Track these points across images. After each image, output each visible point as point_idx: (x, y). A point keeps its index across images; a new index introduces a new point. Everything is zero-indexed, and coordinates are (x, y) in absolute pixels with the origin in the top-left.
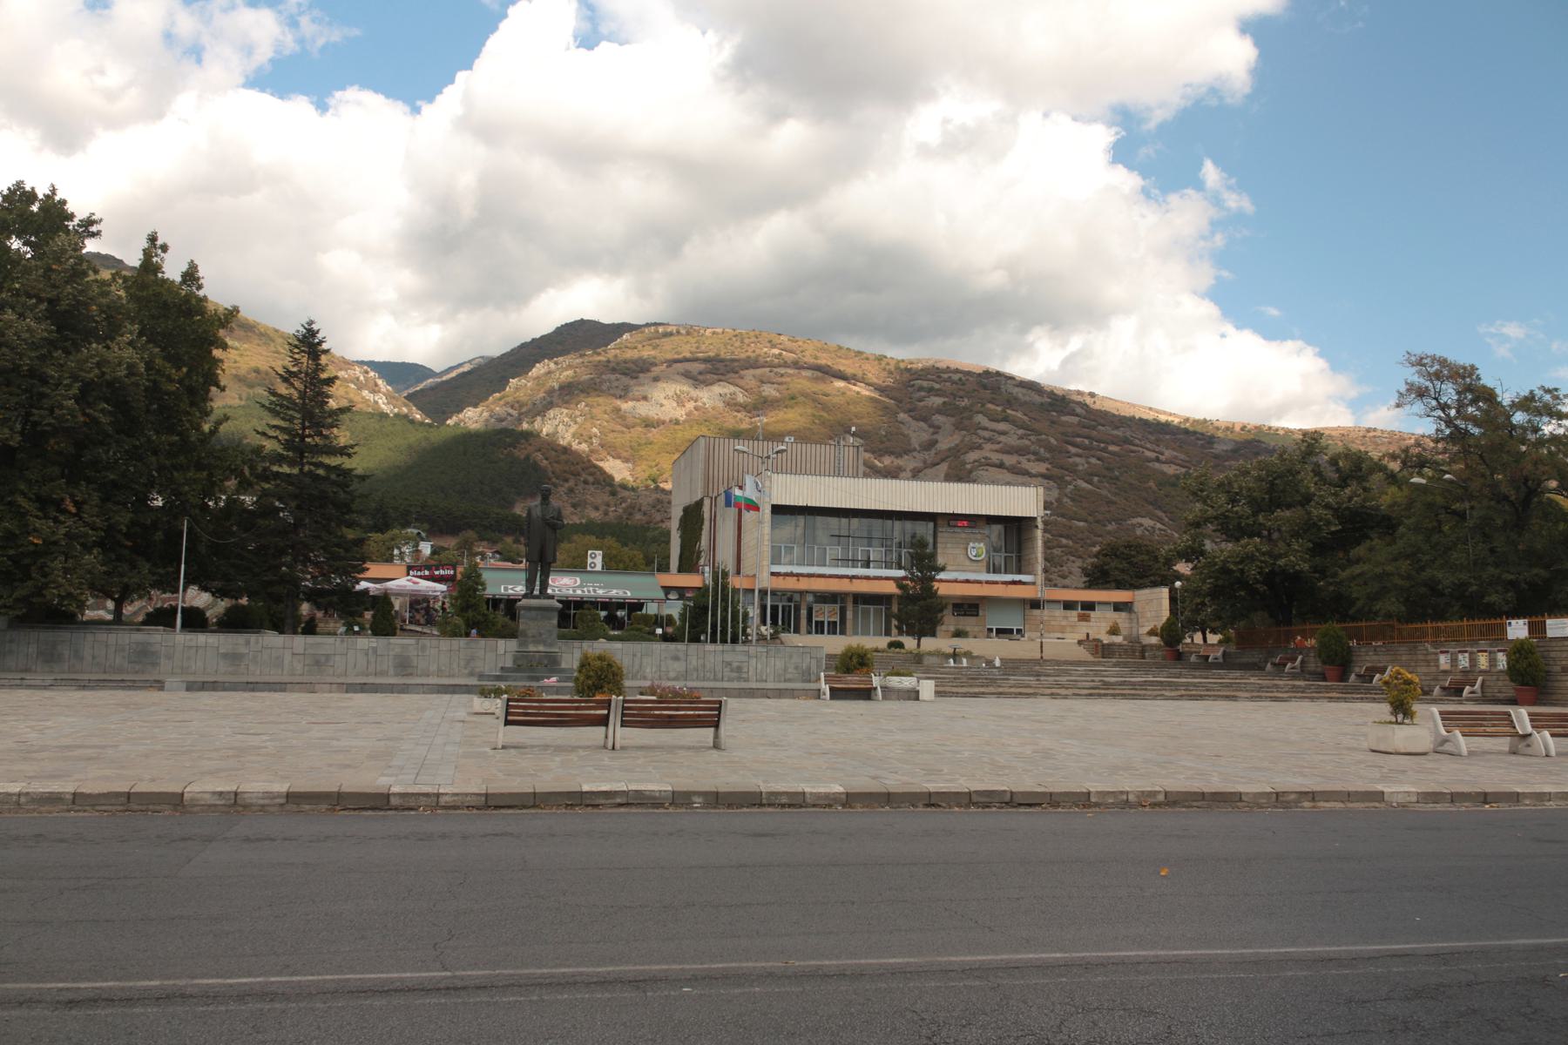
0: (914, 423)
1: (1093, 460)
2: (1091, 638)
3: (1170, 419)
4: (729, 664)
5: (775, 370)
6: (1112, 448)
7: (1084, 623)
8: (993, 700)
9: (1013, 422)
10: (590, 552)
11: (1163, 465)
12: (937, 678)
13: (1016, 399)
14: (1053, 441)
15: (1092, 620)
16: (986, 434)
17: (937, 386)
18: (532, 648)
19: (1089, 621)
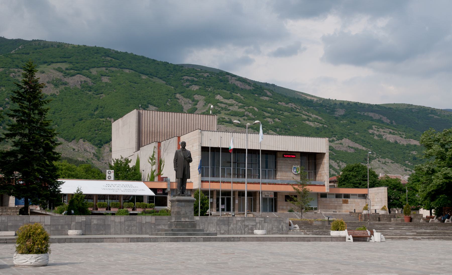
0: (185, 99)
1: (277, 120)
2: (356, 211)
3: (312, 98)
4: (247, 226)
5: (109, 68)
6: (286, 113)
7: (345, 204)
8: (412, 240)
9: (236, 99)
10: (107, 171)
11: (311, 123)
12: (382, 232)
13: (237, 87)
14: (256, 109)
15: (349, 203)
16: (223, 106)
17: (196, 79)
18: (183, 220)
19: (348, 203)
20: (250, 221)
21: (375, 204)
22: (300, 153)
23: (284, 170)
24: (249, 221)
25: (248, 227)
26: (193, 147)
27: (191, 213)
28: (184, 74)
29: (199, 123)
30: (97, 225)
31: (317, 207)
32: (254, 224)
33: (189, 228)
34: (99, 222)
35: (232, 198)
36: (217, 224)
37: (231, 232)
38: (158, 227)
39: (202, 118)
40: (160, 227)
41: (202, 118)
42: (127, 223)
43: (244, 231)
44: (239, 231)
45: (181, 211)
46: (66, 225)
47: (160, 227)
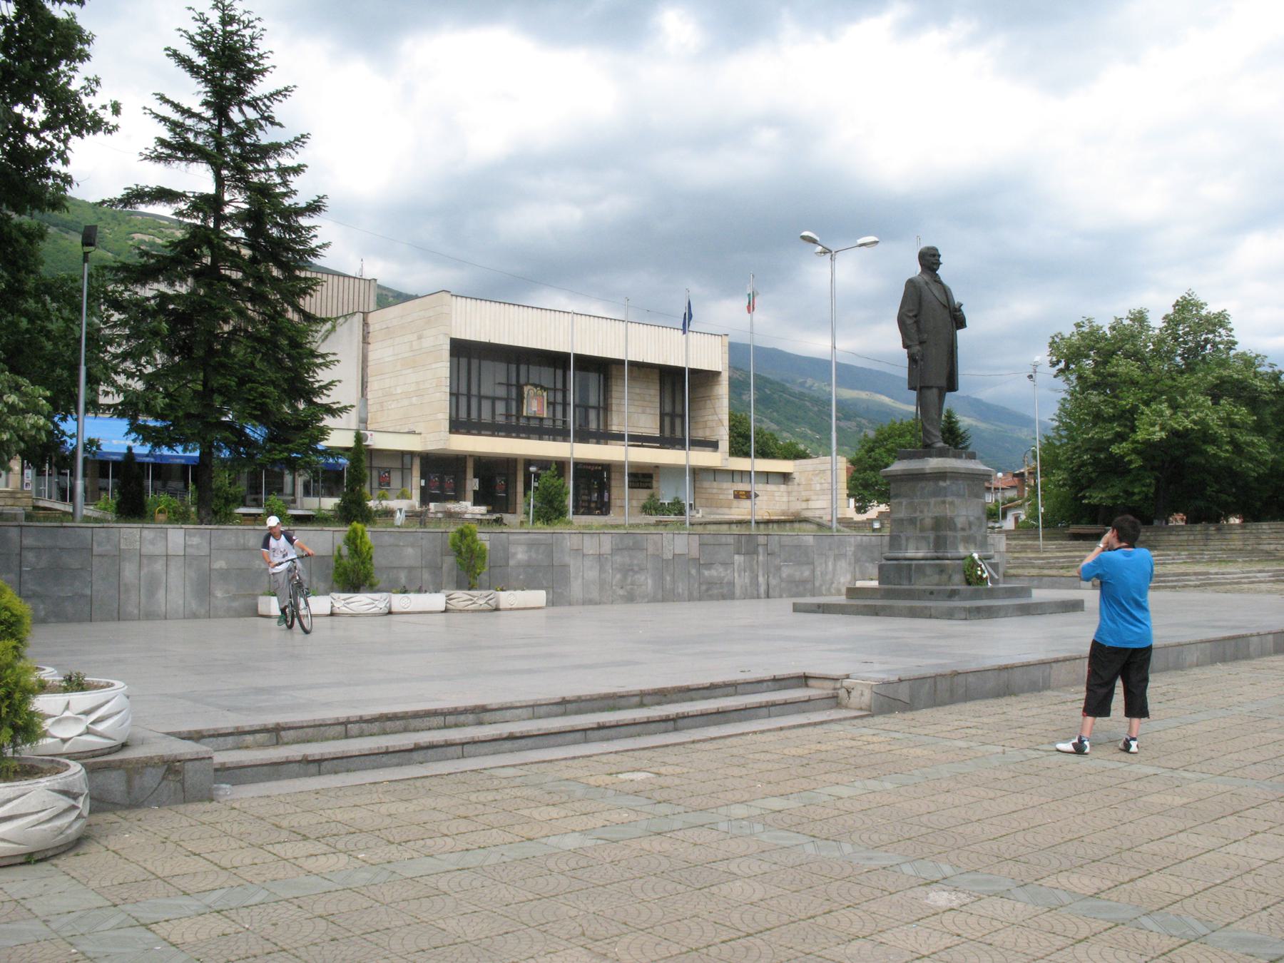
21: (813, 497)
22: (657, 371)
26: (420, 338)
28: (136, 229)
29: (335, 295)
30: (529, 566)
34: (534, 555)
36: (857, 560)
38: (706, 573)
39: (341, 284)
40: (714, 573)
41: (341, 284)
42: (618, 559)
45: (958, 516)
46: (424, 570)
47: (714, 573)
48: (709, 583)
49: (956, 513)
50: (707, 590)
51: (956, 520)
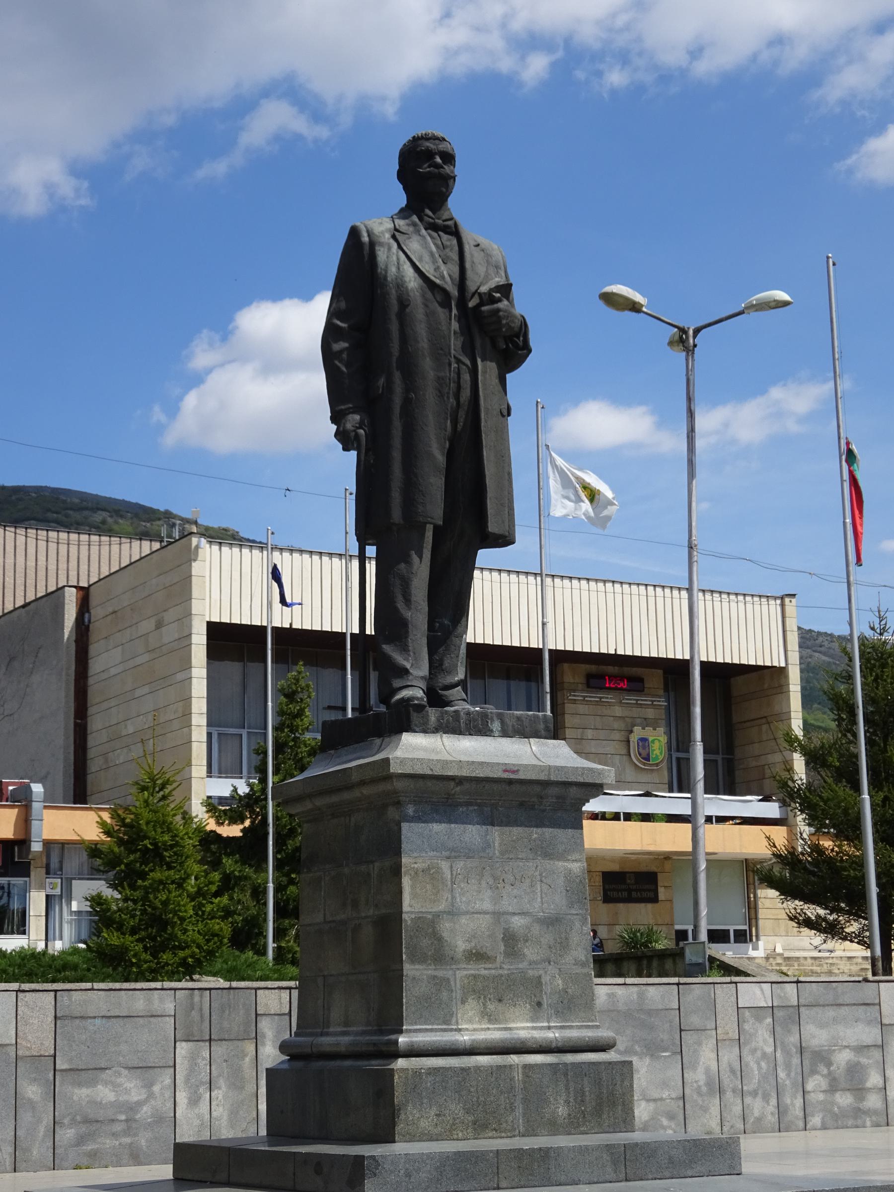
4: (822, 1057)
20: (844, 1011)
23: (593, 750)
24: (831, 1013)
25: (829, 1064)
26: (159, 625)
27: (564, 945)
31: (746, 927)
32: (869, 1041)
33: (554, 1128)
35: (271, 886)
37: (705, 1109)
38: (82, 1093)
40: (105, 1093)
43: (799, 1102)
44: (766, 1098)
45: (453, 913)
47: (105, 1093)
48: (87, 1121)
49: (442, 906)
50: (81, 1140)
51: (445, 927)
